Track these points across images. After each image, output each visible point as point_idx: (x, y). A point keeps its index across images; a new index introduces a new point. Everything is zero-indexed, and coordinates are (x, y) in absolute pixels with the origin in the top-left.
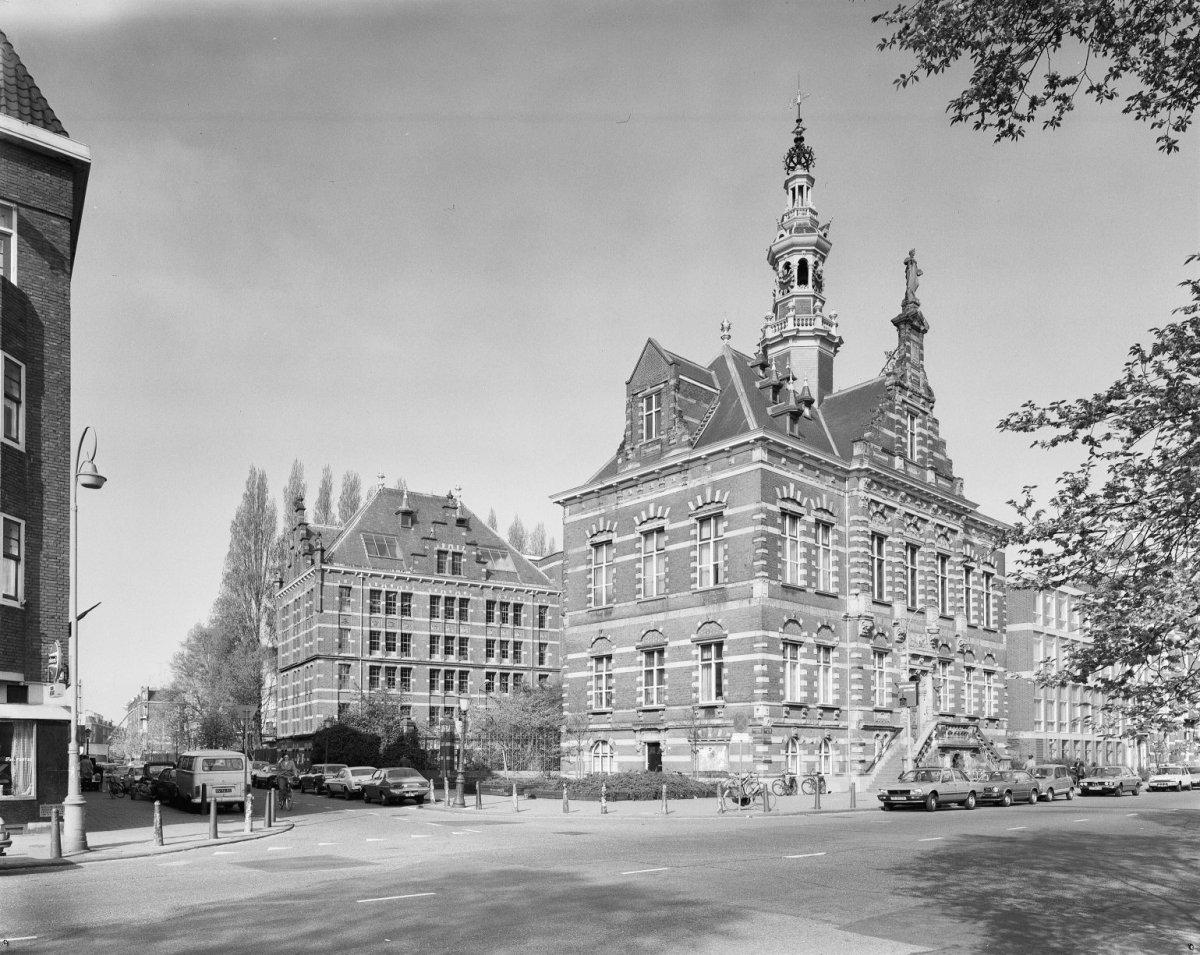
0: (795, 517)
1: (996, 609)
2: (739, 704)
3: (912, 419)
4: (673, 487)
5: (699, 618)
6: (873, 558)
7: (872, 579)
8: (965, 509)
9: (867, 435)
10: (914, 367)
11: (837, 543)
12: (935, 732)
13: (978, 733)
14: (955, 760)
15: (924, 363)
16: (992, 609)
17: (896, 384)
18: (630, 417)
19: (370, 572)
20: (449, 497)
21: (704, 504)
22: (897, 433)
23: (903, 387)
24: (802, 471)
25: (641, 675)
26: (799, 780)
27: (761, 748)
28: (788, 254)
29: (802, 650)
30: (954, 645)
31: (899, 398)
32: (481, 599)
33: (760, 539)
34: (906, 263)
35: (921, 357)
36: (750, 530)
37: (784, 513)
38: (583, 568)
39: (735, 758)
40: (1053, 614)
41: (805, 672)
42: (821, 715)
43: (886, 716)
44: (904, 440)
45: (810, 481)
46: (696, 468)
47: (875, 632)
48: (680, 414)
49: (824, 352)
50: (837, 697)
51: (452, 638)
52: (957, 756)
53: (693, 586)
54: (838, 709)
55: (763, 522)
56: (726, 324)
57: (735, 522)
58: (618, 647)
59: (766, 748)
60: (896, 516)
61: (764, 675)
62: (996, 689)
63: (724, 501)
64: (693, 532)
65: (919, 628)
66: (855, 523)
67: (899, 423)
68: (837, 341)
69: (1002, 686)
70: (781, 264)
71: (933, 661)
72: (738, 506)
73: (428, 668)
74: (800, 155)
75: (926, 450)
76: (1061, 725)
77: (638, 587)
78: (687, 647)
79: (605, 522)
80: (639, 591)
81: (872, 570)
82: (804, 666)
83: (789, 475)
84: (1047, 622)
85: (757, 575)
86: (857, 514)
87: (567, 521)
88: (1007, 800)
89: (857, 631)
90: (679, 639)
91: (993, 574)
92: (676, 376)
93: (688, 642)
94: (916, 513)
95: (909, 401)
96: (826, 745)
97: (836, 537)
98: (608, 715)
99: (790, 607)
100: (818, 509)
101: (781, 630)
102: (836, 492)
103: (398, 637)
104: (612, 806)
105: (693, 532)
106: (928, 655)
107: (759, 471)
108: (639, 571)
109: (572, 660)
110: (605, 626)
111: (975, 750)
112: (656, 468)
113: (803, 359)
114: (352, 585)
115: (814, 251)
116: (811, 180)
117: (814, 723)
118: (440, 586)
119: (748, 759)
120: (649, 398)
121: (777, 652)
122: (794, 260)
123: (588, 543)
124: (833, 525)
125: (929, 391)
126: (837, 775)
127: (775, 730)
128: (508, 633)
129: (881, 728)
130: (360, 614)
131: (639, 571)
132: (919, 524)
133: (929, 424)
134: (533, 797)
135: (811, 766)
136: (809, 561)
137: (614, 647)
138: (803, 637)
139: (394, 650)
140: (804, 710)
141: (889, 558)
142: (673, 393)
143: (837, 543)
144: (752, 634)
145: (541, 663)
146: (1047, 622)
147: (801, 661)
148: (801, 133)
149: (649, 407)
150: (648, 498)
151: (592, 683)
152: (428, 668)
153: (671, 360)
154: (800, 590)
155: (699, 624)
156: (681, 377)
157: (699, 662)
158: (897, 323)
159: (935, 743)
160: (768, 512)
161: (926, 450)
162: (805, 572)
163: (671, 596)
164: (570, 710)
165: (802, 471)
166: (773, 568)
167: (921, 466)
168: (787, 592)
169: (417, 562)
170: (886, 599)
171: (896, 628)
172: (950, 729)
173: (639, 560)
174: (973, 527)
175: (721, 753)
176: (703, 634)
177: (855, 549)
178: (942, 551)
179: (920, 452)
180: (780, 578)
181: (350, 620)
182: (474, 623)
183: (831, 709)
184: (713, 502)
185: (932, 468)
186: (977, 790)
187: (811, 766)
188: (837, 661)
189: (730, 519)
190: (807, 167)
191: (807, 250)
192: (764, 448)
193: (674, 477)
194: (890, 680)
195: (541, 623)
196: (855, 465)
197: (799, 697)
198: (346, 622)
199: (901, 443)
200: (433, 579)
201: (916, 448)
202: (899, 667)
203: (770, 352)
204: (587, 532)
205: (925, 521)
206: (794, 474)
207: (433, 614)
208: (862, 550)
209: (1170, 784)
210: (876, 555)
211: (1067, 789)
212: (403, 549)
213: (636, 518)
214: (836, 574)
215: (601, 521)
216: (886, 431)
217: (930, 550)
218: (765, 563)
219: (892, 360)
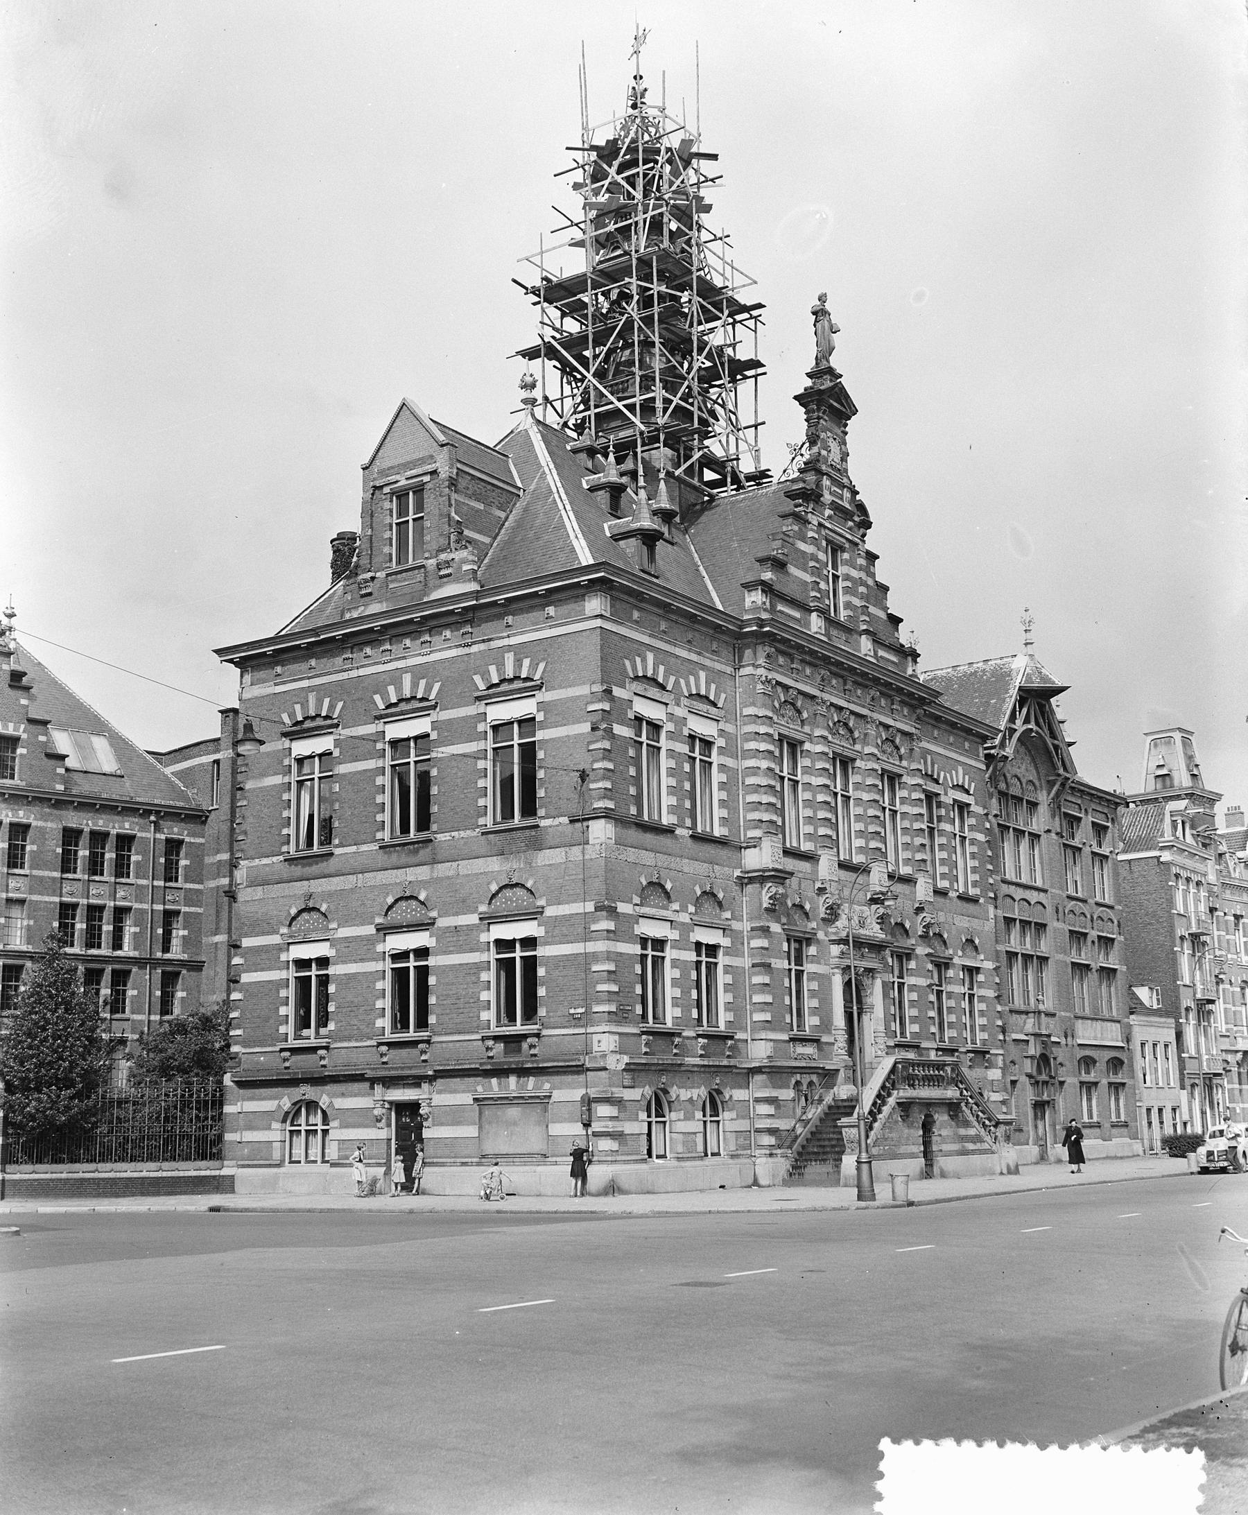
13: (958, 1080)
30: (814, 909)
38: (278, 780)
43: (809, 1050)
50: (730, 1017)
72: (561, 687)
75: (857, 602)
86: (753, 704)
89: (761, 904)
90: (457, 914)
95: (827, 525)
101: (637, 900)
111: (953, 1108)
120: (401, 495)
125: (861, 508)
126: (733, 1157)
137: (333, 925)
145: (166, 949)
149: (403, 511)
161: (857, 602)
164: (245, 1044)
171: (822, 899)
177: (751, 763)
179: (848, 605)
182: (35, 872)
184: (517, 678)
185: (867, 632)
195: (170, 873)
199: (819, 591)
201: (842, 599)
213: (377, 698)
215: (312, 699)
219: (799, 457)
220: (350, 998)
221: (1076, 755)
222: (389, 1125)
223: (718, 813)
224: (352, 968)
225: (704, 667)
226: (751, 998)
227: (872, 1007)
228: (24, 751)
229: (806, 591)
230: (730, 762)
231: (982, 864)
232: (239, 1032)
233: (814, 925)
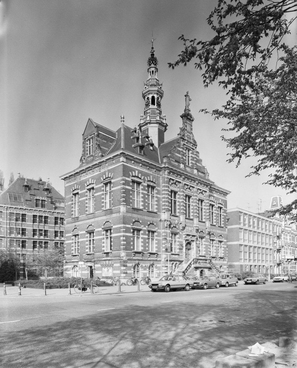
0: (139, 183)
2: (116, 252)
3: (189, 151)
4: (96, 172)
5: (104, 220)
6: (199, 207)
7: (186, 211)
8: (209, 184)
9: (169, 155)
10: (188, 132)
11: (157, 193)
12: (193, 262)
14: (201, 272)
15: (193, 131)
16: (222, 220)
17: (181, 138)
18: (84, 147)
19: (9, 206)
20: (40, 180)
21: (106, 178)
22: (182, 155)
23: (183, 139)
24: (141, 166)
25: (87, 241)
26: (139, 279)
27: (123, 268)
28: (148, 94)
29: (141, 232)
30: (205, 232)
31: (182, 143)
32: (53, 216)
33: (122, 190)
34: (185, 96)
35: (192, 129)
36: (119, 187)
37: (133, 182)
38: (70, 203)
39: (115, 272)
40: (247, 222)
41: (142, 240)
42: (150, 256)
43: (177, 256)
44: (184, 158)
45: (145, 170)
46: (103, 165)
47: (172, 226)
48: (99, 145)
49: (161, 128)
50: (157, 249)
51: (42, 230)
52: (202, 270)
53: (102, 209)
54: (157, 254)
55: (124, 184)
56: (122, 116)
57: (116, 184)
58: (80, 231)
59: (125, 268)
60: (181, 185)
61: (124, 241)
62: (223, 247)
63: (112, 177)
64: (102, 189)
65: (191, 225)
66: (164, 186)
67: (182, 152)
68: (165, 125)
69: (226, 246)
70: (146, 98)
71: (196, 237)
73: (32, 240)
75: (194, 162)
76: (263, 261)
77: (86, 209)
78: (101, 231)
80: (87, 211)
81: (199, 211)
82: (142, 238)
83: (136, 168)
84: (244, 225)
85: (122, 204)
86: (164, 183)
87: (66, 186)
88: (205, 287)
91: (222, 208)
92: (97, 131)
93: (101, 229)
96: (221, 267)
97: (156, 191)
98: (77, 256)
99: (136, 216)
100: (148, 181)
101: (132, 224)
102: (156, 175)
104: (48, 290)
105: (102, 189)
106: (188, 234)
107: (122, 165)
108: (87, 203)
110: (77, 224)
112: (90, 165)
113: (153, 132)
114: (2, 211)
115: (157, 93)
116: (157, 69)
117: (146, 259)
118: (37, 211)
119: (118, 272)
121: (130, 232)
122: (150, 96)
123: (72, 194)
124: (155, 187)
125: (195, 141)
126: (156, 278)
127: (129, 261)
128: (42, 226)
129: (174, 261)
130: (6, 221)
131: (87, 203)
132: (191, 188)
133: (195, 153)
134: (25, 287)
135: (145, 274)
136: (145, 200)
138: (142, 227)
140: (142, 254)
141: (204, 207)
142: (96, 138)
143: (157, 193)
146: (244, 225)
147: (141, 236)
148: (153, 52)
150: (89, 177)
151: (74, 245)
152: (32, 240)
153: (95, 126)
154: (141, 210)
155: (104, 222)
156: (99, 132)
157: (105, 237)
158: (182, 117)
159: (193, 266)
160: (126, 181)
161: (194, 162)
162: (143, 203)
163: (96, 212)
164: (67, 255)
165: (141, 166)
166: (127, 201)
167: (192, 168)
168: (134, 210)
169: (27, 203)
170: (204, 220)
171: (181, 225)
172: (200, 261)
173: (87, 199)
174: (214, 191)
175: (111, 270)
176: (105, 226)
177: (164, 196)
178: (200, 198)
179: (192, 163)
180: (131, 205)
182: (50, 225)
183: (222, 258)
185: (196, 169)
186: (190, 283)
187: (145, 274)
189: (114, 183)
190: (155, 65)
191: (154, 93)
192: (124, 157)
193: (97, 169)
194: (178, 243)
196: (163, 166)
197: (140, 249)
199: (183, 159)
200: (34, 209)
201: (190, 161)
202: (181, 239)
203: (142, 128)
204: (71, 190)
205: (194, 187)
206: (138, 168)
207: (34, 221)
208: (166, 196)
209: (280, 280)
210: (200, 206)
211: (235, 282)
212: (24, 198)
213: (85, 184)
214: (157, 205)
215: (75, 185)
216: (177, 154)
217: (195, 198)
218: (124, 199)
221: (216, 183)
223: (156, 207)
225: (221, 199)
227: (193, 248)
231: (225, 220)
233: (179, 231)
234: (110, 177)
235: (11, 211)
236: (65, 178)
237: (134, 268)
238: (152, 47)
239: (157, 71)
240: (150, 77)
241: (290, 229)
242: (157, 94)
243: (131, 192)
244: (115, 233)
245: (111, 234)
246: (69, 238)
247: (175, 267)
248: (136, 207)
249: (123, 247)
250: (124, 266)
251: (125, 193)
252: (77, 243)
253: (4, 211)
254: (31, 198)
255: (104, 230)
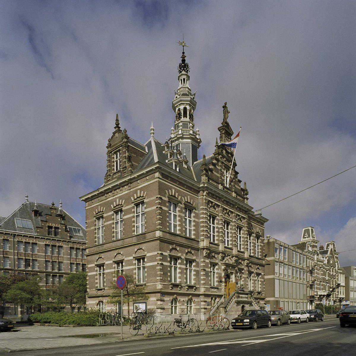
1: (261, 254)
4: (125, 191)
29: (179, 261)
43: (215, 290)
44: (223, 178)
54: (195, 287)
55: (160, 204)
59: (162, 303)
68: (199, 141)
69: (263, 280)
70: (177, 109)
73: (45, 274)
74: (184, 66)
78: (131, 260)
79: (101, 208)
94: (228, 208)
103: (31, 261)
109: (90, 267)
116: (188, 77)
122: (182, 107)
136: (182, 223)
139: (30, 266)
144: (156, 253)
164: (89, 289)
169: (38, 230)
181: (8, 253)
188: (194, 267)
190: (187, 72)
191: (186, 104)
198: (7, 254)
199: (222, 179)
204: (94, 212)
213: (112, 205)
214: (194, 230)
220: (108, 278)
222: (117, 306)
224: (109, 271)
226: (200, 278)
228: (60, 230)
229: (218, 179)
230: (196, 220)
232: (88, 286)
234: (143, 196)
235: (19, 239)
236: (86, 199)
237: (172, 303)
238: (183, 52)
239: (189, 80)
240: (180, 86)
241: (322, 264)
242: (190, 105)
243: (167, 214)
244: (149, 263)
245: (104, 270)
246: (92, 269)
247: (214, 302)
248: (173, 231)
249: (159, 278)
250: (161, 300)
251: (162, 214)
252: (102, 274)
253: (11, 239)
254: (43, 224)
255: (136, 259)
